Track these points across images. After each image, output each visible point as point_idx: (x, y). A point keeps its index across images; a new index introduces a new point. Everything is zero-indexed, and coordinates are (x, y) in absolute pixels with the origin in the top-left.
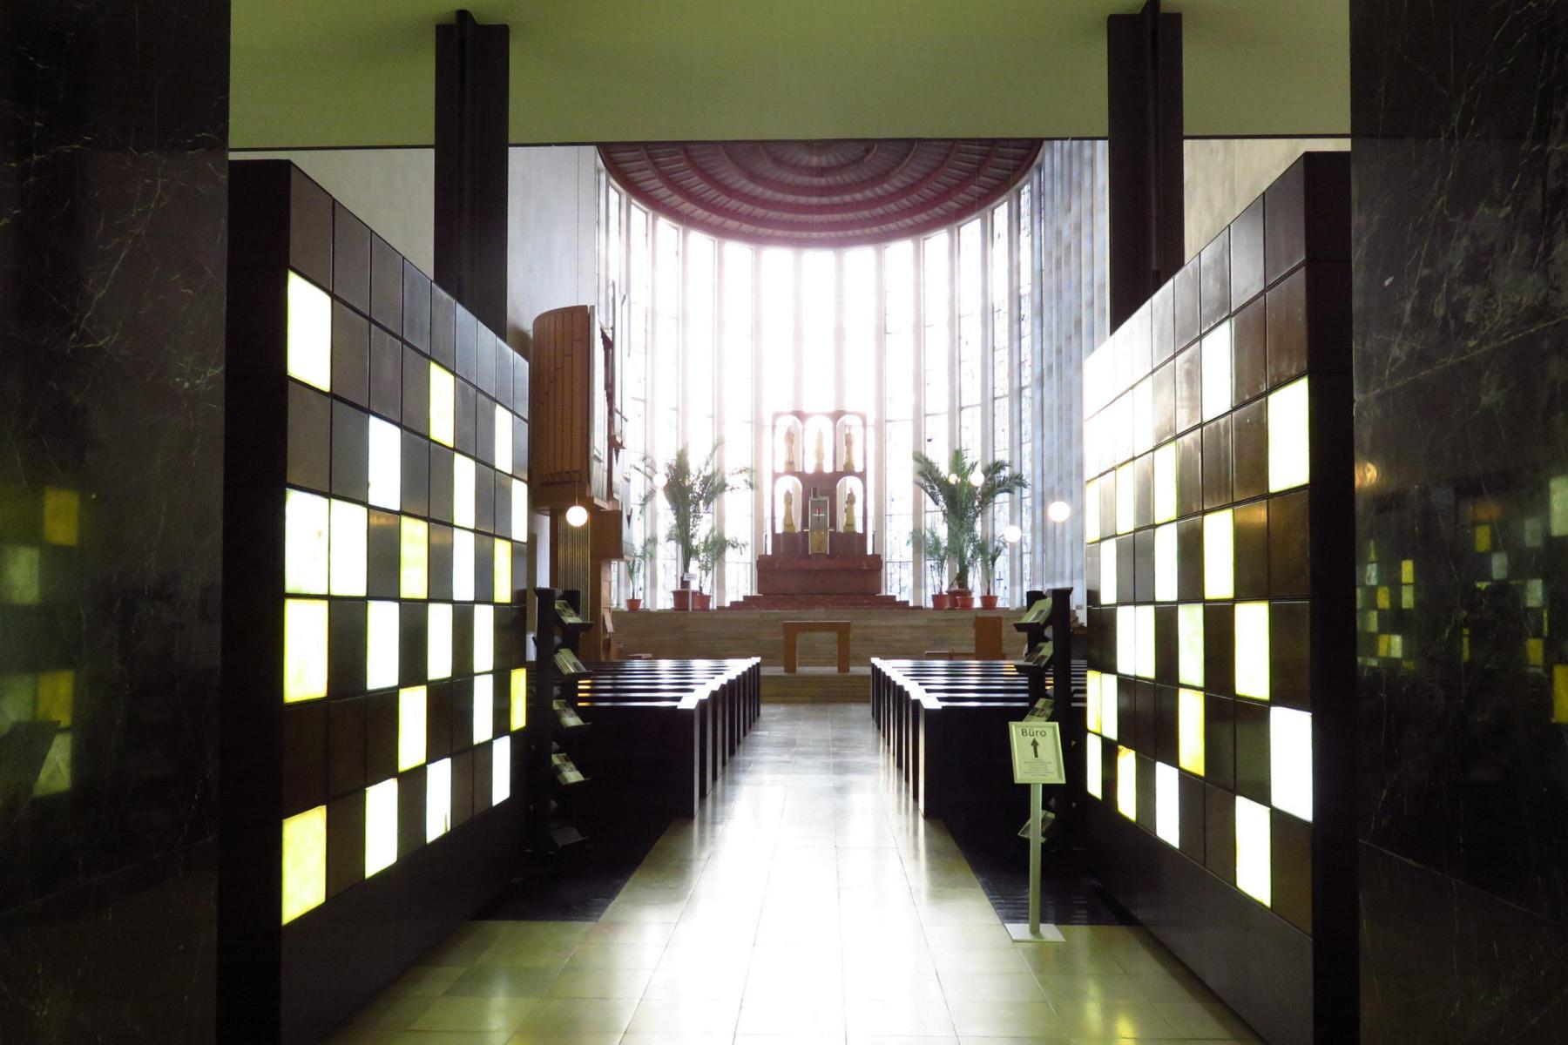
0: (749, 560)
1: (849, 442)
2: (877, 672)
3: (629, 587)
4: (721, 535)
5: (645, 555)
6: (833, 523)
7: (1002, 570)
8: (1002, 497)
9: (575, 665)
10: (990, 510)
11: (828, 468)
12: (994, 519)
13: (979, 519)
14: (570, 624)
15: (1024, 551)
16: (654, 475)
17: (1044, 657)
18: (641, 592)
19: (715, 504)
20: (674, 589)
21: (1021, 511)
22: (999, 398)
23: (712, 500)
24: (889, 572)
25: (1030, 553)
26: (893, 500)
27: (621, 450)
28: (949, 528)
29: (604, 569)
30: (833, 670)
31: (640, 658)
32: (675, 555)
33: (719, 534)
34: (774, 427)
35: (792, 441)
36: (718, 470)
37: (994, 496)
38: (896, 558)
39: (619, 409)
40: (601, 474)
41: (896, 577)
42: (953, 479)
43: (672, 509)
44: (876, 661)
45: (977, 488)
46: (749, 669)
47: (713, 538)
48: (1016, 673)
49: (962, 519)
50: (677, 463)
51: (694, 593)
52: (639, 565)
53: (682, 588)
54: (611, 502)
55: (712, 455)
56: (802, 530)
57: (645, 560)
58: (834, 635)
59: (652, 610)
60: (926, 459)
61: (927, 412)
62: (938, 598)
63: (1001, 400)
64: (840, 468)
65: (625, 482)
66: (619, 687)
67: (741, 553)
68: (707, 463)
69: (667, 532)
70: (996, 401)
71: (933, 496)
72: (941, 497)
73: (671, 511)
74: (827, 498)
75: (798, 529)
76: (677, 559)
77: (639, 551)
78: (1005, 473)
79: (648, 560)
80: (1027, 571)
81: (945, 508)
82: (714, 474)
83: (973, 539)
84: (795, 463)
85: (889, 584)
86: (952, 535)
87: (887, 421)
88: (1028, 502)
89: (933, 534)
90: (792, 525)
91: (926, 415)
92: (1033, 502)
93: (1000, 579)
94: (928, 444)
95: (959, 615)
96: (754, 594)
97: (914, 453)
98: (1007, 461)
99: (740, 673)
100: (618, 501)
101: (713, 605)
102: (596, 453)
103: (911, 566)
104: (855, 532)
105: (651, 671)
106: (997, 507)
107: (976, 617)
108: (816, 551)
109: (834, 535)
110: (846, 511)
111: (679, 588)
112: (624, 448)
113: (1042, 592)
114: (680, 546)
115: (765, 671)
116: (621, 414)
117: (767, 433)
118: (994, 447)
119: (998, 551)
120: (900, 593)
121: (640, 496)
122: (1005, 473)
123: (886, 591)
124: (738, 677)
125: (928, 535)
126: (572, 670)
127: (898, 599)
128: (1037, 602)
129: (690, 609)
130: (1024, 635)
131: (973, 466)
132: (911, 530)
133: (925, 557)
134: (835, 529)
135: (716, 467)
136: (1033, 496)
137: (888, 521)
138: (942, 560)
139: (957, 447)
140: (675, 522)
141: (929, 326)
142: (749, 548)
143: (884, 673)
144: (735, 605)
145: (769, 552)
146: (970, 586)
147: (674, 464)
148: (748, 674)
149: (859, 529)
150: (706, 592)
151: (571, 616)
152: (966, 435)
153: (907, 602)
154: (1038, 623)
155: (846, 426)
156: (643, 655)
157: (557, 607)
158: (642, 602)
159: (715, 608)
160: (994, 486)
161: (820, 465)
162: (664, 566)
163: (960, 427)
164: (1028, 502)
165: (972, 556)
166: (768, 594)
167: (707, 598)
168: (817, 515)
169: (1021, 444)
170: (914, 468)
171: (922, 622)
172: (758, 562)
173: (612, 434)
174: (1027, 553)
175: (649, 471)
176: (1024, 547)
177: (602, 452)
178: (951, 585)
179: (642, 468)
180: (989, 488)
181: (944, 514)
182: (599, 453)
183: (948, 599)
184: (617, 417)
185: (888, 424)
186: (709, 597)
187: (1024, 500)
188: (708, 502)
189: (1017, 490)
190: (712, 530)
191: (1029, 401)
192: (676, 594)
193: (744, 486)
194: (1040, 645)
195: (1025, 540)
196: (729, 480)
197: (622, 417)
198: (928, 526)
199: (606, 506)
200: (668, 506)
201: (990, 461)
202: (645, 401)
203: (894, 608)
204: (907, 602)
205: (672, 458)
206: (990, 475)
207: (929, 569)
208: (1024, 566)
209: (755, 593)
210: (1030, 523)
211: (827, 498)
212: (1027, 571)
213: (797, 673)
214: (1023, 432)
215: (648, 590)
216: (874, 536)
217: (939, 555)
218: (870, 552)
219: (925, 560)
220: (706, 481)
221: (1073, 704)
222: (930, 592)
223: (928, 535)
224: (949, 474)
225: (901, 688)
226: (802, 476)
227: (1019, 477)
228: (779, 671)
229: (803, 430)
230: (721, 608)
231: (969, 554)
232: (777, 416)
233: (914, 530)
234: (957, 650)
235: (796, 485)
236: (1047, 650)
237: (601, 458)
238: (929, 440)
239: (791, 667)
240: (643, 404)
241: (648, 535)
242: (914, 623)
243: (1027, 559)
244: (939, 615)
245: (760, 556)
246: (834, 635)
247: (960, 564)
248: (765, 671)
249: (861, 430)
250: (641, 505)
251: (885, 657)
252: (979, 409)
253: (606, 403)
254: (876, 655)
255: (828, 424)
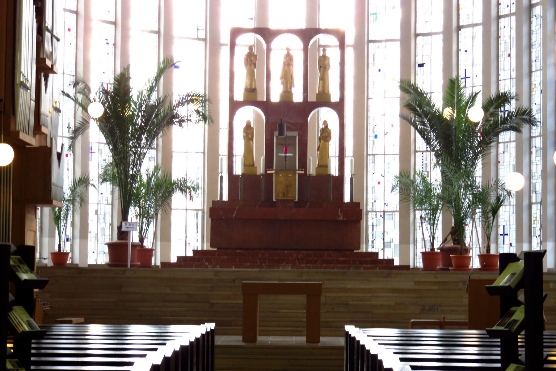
0: (200, 207)
1: (324, 65)
2: (351, 340)
3: (54, 236)
4: (167, 175)
5: (74, 199)
6: (303, 164)
7: (507, 223)
8: (505, 136)
9: (29, 324)
10: (493, 151)
11: (298, 97)
12: (498, 162)
13: (479, 162)
14: (25, 280)
15: (534, 200)
16: (88, 105)
17: (515, 321)
18: (68, 244)
19: (160, 140)
20: (109, 241)
21: (531, 153)
22: (505, 16)
23: (156, 134)
24: (370, 223)
25: (541, 203)
26: (376, 136)
27: (51, 75)
28: (443, 172)
29: (29, 217)
30: (300, 340)
31: (70, 322)
32: (110, 199)
33: (164, 174)
34: (233, 46)
35: (255, 64)
36: (165, 97)
37: (497, 135)
38: (379, 207)
39: (50, 28)
40: (28, 104)
41: (379, 230)
42: (447, 113)
43: (108, 143)
44: (351, 329)
45: (476, 124)
46: (203, 335)
47: (157, 179)
48: (488, 336)
49: (459, 162)
50: (115, 89)
51: (134, 246)
52: (67, 210)
53: (119, 238)
54: (37, 136)
55: (157, 80)
56: (266, 171)
57: (74, 205)
58: (302, 299)
59: (81, 265)
60: (416, 89)
61: (418, 32)
62: (428, 256)
63: (507, 19)
64: (312, 98)
65: (54, 112)
66: (43, 351)
67: (191, 198)
68: (151, 89)
69: (101, 171)
70: (502, 21)
71: (423, 133)
72: (432, 135)
73: (107, 147)
74: (295, 134)
75: (261, 169)
76: (112, 204)
77: (67, 193)
78: (511, 107)
79: (77, 205)
80: (537, 225)
81: (438, 147)
82: (160, 102)
83: (471, 186)
84: (258, 90)
85: (370, 239)
86: (446, 181)
87: (369, 42)
88: (537, 142)
89: (424, 179)
90: (253, 165)
91: (417, 35)
92: (545, 142)
93: (504, 235)
94: (418, 69)
95: (452, 277)
96: (205, 249)
97: (402, 82)
98: (513, 91)
99: (193, 340)
100: (46, 135)
101: (156, 261)
102: (22, 79)
103: (397, 216)
104: (330, 176)
105: (80, 336)
106: (501, 146)
107: (470, 280)
108: (281, 197)
109: (304, 178)
110: (318, 150)
111: (115, 239)
112: (54, 73)
113: (515, 255)
114: (117, 189)
115: (220, 340)
116: (51, 32)
117: (225, 52)
118: (498, 75)
119: (499, 203)
120: (383, 249)
121: (69, 127)
122: (511, 107)
123: (367, 247)
124: (191, 343)
125: (418, 180)
126: (27, 329)
127: (381, 257)
128: (510, 264)
129: (129, 266)
130: (497, 299)
131: (473, 98)
132: (397, 173)
133: (414, 207)
134: (306, 171)
135: (161, 95)
136: (544, 135)
137: (370, 161)
138: (434, 210)
139: (454, 76)
140: (110, 159)
141: (370, 99)
142: (200, 192)
143: (359, 342)
144: (182, 260)
145: (225, 198)
146: (467, 241)
147: (111, 89)
148: (195, 344)
149: (334, 171)
150: (148, 244)
151: (26, 272)
152: (465, 62)
153: (392, 261)
154: (509, 286)
155: (320, 46)
156: (74, 319)
157: (12, 263)
158: (70, 255)
159: (158, 263)
160: (496, 123)
161: (287, 93)
162: (97, 212)
163: (458, 50)
164: (537, 142)
165: (469, 207)
166: (221, 248)
167: (149, 253)
168: (283, 154)
169: (530, 72)
170: (402, 99)
171: (408, 284)
172: (211, 209)
173: (42, 56)
174: (536, 203)
175: (80, 97)
176: (533, 195)
177: (29, 79)
178: (445, 241)
179: (72, 94)
180: (491, 126)
181: (437, 156)
182: (27, 79)
183: (440, 257)
184: (48, 36)
185: (371, 45)
186: (151, 251)
187: (533, 139)
188: (152, 137)
189: (525, 128)
190: (156, 169)
191: (539, 21)
192: (111, 246)
193: (195, 117)
194: (513, 309)
195: (535, 187)
196: (182, 111)
197: (53, 36)
198: (419, 167)
199: (32, 141)
200: (103, 139)
201: (493, 92)
202: (76, 13)
203: (375, 268)
204: (392, 261)
205: (109, 81)
206: (492, 110)
207: (419, 221)
208: (533, 219)
209: (207, 247)
210: (540, 168)
211: (295, 134)
212: (537, 225)
213: (258, 343)
214: (533, 58)
215: (77, 241)
216: (352, 179)
217: (430, 205)
218: (347, 199)
219: (414, 211)
220: (151, 111)
221: (546, 366)
222: (420, 248)
223: (418, 180)
224: (443, 109)
225: (376, 356)
226: (266, 106)
227: (529, 112)
228: (236, 340)
229: (269, 50)
230: (166, 265)
231: (466, 204)
232: (236, 33)
233: (401, 174)
234: (450, 318)
235: (258, 115)
236: (519, 315)
237: (29, 85)
238: (421, 65)
239: (250, 337)
240: (75, 16)
241: (78, 174)
242: (397, 285)
243: (536, 211)
244: (430, 277)
245: (213, 202)
246: (302, 299)
247: (455, 216)
248: (220, 340)
249: (338, 51)
250: (71, 138)
251: (361, 324)
252: (479, 30)
253: (35, 20)
254: (350, 323)
255: (296, 44)
